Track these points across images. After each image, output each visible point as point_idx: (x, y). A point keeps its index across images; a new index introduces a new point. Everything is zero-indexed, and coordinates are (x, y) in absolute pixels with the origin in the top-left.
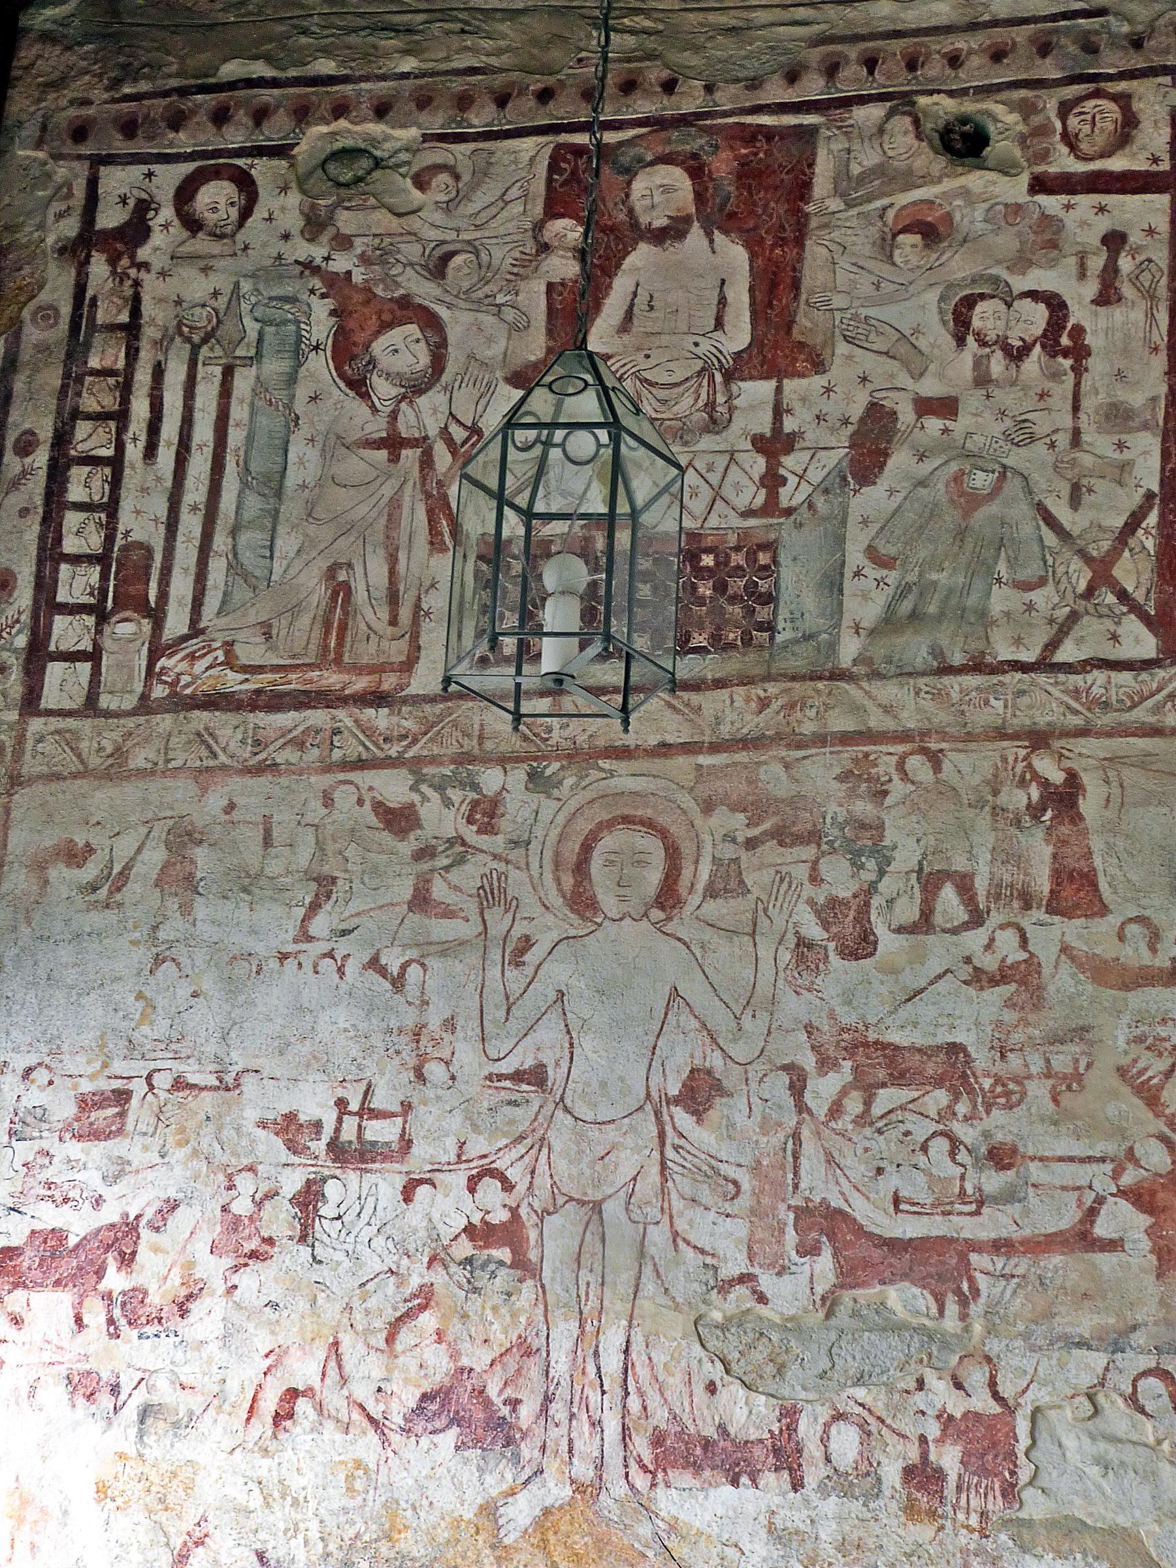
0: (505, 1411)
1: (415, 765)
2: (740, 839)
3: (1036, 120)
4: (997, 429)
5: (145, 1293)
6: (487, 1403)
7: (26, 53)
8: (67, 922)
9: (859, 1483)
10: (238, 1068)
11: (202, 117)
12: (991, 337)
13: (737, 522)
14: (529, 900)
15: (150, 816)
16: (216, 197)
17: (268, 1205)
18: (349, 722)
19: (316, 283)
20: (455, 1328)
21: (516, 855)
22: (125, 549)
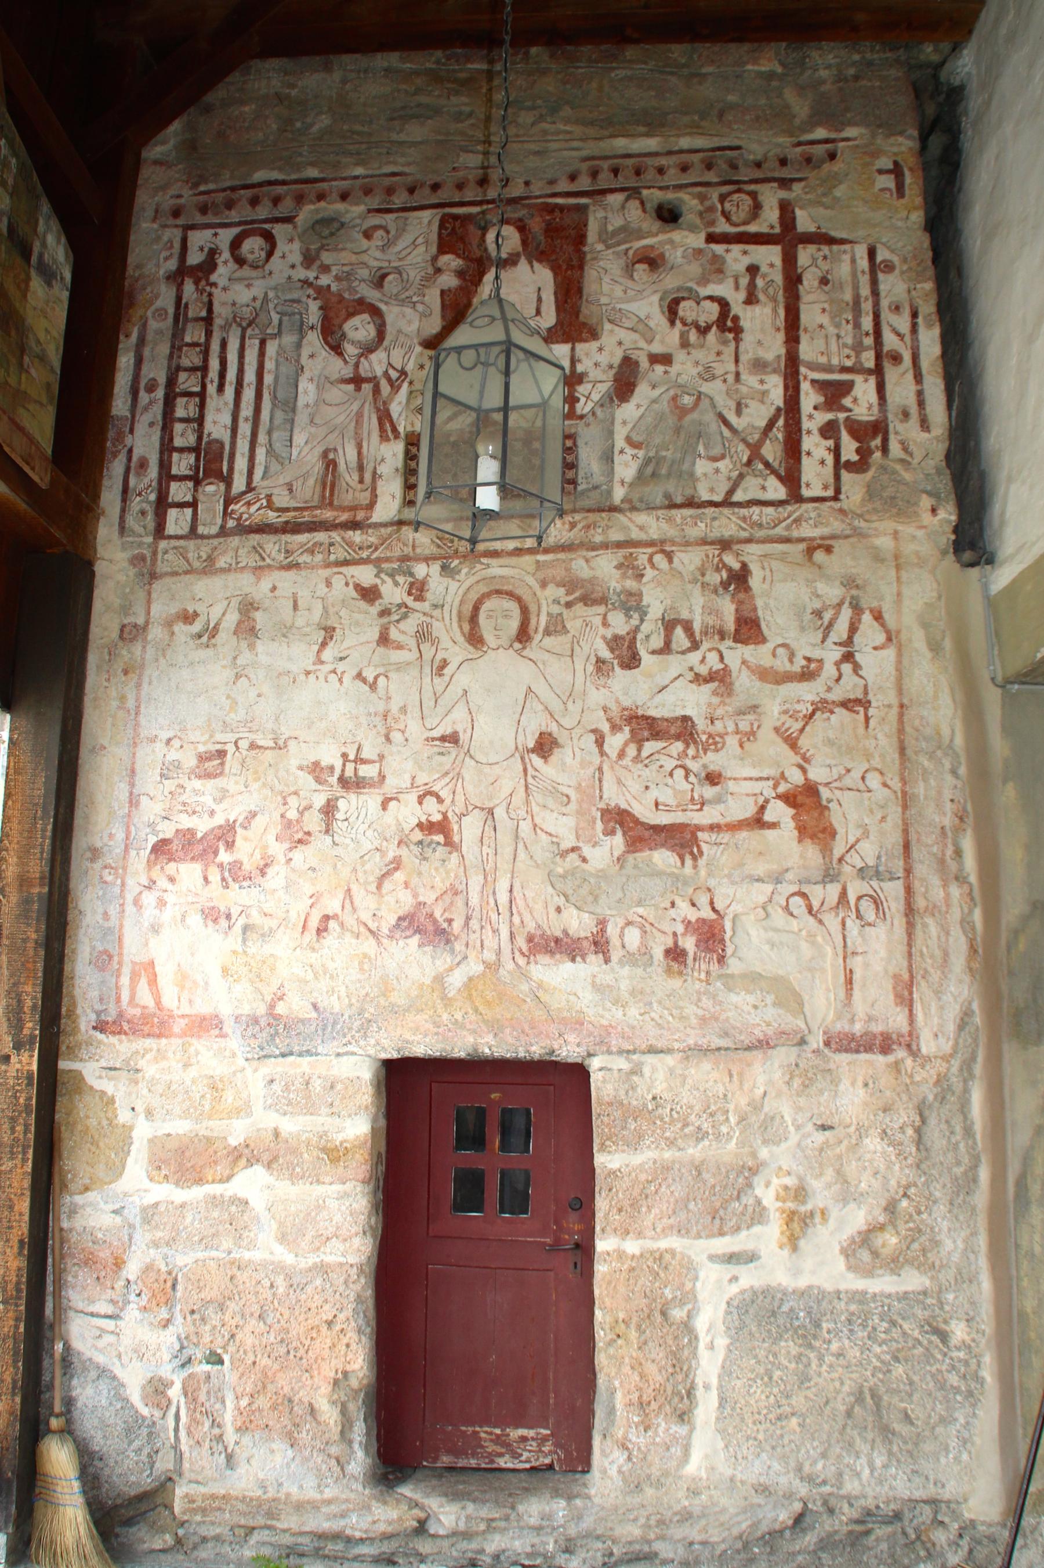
0: (445, 925)
3: (708, 203)
4: (694, 371)
6: (435, 921)
7: (145, 172)
9: (641, 957)
11: (244, 202)
12: (689, 320)
16: (253, 246)
19: (311, 291)
20: (415, 881)
21: (437, 613)
22: (209, 443)
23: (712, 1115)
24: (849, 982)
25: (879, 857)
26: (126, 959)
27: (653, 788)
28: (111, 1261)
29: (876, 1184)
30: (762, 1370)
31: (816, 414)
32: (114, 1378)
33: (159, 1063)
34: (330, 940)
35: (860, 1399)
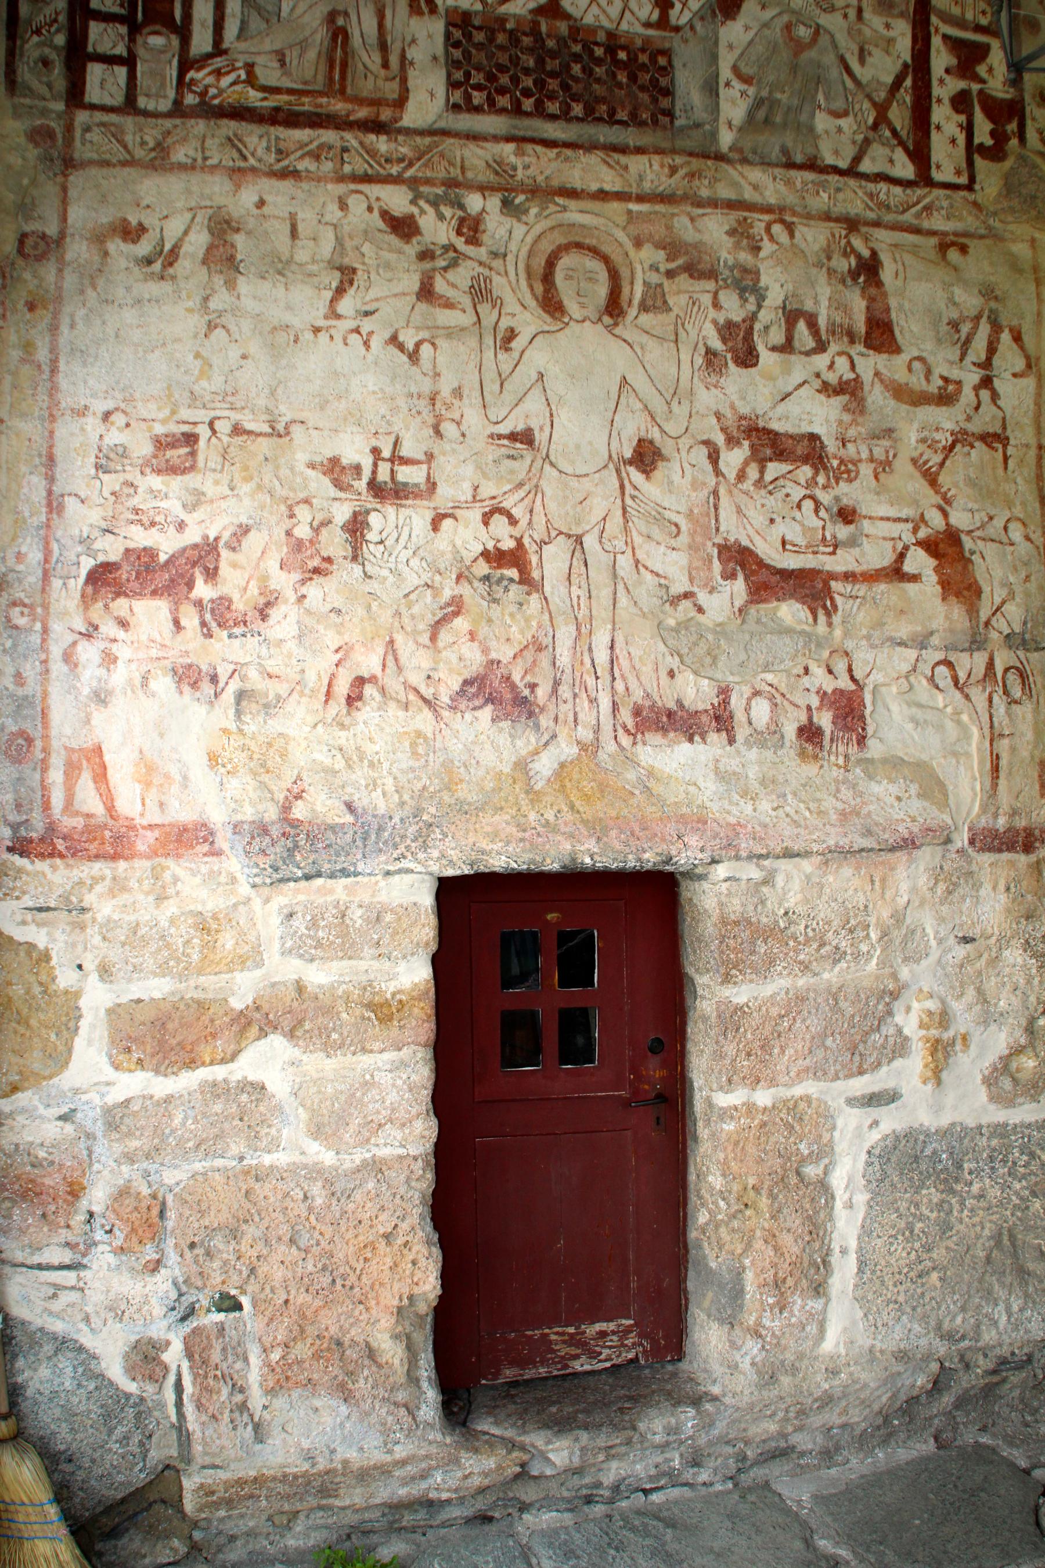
0: (526, 692)
1: (413, 183)
2: (662, 269)
5: (230, 601)
6: (513, 687)
8: (128, 289)
10: (287, 418)
13: (641, 30)
14: (509, 298)
15: (193, 204)
17: (324, 531)
18: (355, 143)
20: (483, 631)
21: (497, 263)
23: (851, 931)
24: (996, 769)
25: (1025, 623)
26: (55, 744)
27: (777, 523)
28: (63, 1188)
29: (1016, 1001)
30: (902, 1224)
31: (948, 79)
32: (81, 1349)
33: (117, 898)
34: (367, 713)
35: (997, 1238)
